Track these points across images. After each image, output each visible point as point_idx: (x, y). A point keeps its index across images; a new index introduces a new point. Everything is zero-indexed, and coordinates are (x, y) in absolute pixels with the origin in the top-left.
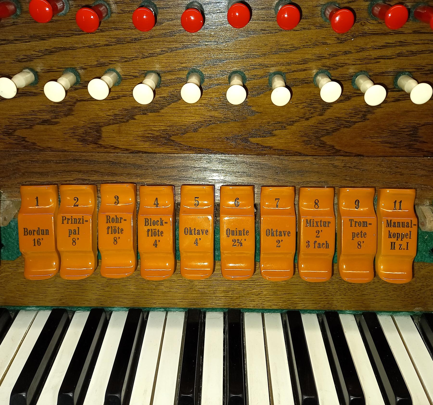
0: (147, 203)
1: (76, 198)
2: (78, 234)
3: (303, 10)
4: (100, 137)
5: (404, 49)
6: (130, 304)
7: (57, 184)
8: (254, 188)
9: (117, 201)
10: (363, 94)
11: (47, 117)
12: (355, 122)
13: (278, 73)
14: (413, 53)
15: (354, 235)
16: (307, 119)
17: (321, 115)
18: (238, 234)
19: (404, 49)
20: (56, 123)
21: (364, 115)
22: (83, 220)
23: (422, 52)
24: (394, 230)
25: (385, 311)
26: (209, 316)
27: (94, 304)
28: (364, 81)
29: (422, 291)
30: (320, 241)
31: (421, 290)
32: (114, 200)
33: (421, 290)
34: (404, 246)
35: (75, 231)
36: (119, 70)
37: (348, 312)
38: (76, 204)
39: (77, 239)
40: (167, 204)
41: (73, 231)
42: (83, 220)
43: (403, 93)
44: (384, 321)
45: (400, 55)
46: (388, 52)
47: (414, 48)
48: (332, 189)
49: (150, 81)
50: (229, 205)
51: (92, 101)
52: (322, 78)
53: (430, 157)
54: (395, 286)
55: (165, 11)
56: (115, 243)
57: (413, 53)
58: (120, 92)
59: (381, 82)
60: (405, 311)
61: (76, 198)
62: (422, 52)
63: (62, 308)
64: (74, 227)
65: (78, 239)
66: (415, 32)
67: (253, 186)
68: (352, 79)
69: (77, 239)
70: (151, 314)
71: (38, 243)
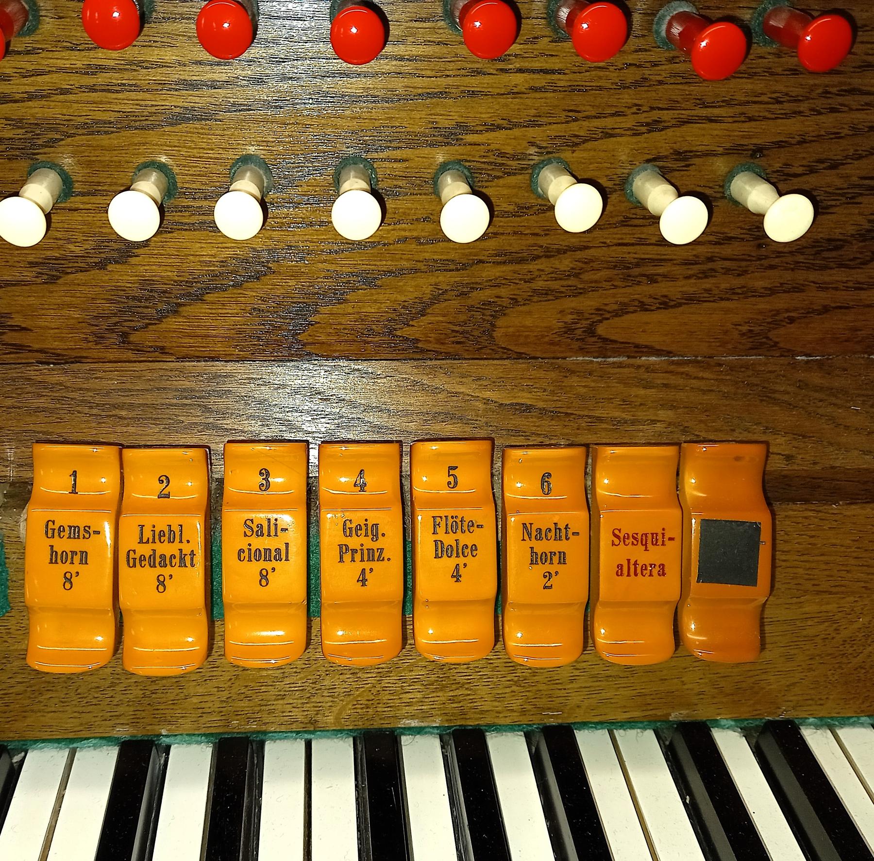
0: (143, 489)
1: (163, 478)
2: (287, 559)
3: (385, 8)
6: (214, 723)
7: (679, 444)
8: (401, 446)
9: (264, 482)
10: (655, 220)
13: (263, 166)
18: (366, 558)
22: (276, 529)
25: (44, 741)
26: (271, 749)
28: (154, 183)
29: (118, 688)
31: (113, 685)
32: (260, 479)
33: (113, 685)
35: (278, 550)
36: (67, 162)
37: (864, 719)
38: (166, 492)
39: (167, 578)
40: (190, 487)
41: (273, 553)
42: (276, 529)
44: (591, 745)
48: (486, 445)
49: (148, 187)
50: (339, 487)
51: (665, 245)
52: (454, 180)
53: (53, 363)
54: (47, 678)
55: (528, 21)
56: (264, 582)
59: (689, 190)
60: (95, 738)
61: (163, 478)
63: (235, 735)
65: (171, 576)
67: (400, 443)
68: (625, 182)
69: (167, 578)
70: (269, 747)
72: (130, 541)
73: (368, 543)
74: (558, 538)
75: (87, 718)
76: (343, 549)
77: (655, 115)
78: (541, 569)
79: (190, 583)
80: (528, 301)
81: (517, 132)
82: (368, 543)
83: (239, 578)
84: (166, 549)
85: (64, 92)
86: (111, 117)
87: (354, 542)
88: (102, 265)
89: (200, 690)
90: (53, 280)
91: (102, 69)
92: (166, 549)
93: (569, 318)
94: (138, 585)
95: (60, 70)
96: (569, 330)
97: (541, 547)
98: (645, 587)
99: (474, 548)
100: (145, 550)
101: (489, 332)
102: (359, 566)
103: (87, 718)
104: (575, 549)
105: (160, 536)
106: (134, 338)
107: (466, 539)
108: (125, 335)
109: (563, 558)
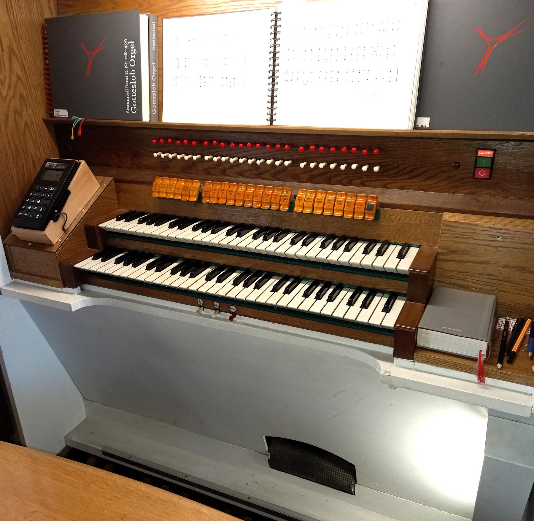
11: (214, 166)
104: (353, 205)
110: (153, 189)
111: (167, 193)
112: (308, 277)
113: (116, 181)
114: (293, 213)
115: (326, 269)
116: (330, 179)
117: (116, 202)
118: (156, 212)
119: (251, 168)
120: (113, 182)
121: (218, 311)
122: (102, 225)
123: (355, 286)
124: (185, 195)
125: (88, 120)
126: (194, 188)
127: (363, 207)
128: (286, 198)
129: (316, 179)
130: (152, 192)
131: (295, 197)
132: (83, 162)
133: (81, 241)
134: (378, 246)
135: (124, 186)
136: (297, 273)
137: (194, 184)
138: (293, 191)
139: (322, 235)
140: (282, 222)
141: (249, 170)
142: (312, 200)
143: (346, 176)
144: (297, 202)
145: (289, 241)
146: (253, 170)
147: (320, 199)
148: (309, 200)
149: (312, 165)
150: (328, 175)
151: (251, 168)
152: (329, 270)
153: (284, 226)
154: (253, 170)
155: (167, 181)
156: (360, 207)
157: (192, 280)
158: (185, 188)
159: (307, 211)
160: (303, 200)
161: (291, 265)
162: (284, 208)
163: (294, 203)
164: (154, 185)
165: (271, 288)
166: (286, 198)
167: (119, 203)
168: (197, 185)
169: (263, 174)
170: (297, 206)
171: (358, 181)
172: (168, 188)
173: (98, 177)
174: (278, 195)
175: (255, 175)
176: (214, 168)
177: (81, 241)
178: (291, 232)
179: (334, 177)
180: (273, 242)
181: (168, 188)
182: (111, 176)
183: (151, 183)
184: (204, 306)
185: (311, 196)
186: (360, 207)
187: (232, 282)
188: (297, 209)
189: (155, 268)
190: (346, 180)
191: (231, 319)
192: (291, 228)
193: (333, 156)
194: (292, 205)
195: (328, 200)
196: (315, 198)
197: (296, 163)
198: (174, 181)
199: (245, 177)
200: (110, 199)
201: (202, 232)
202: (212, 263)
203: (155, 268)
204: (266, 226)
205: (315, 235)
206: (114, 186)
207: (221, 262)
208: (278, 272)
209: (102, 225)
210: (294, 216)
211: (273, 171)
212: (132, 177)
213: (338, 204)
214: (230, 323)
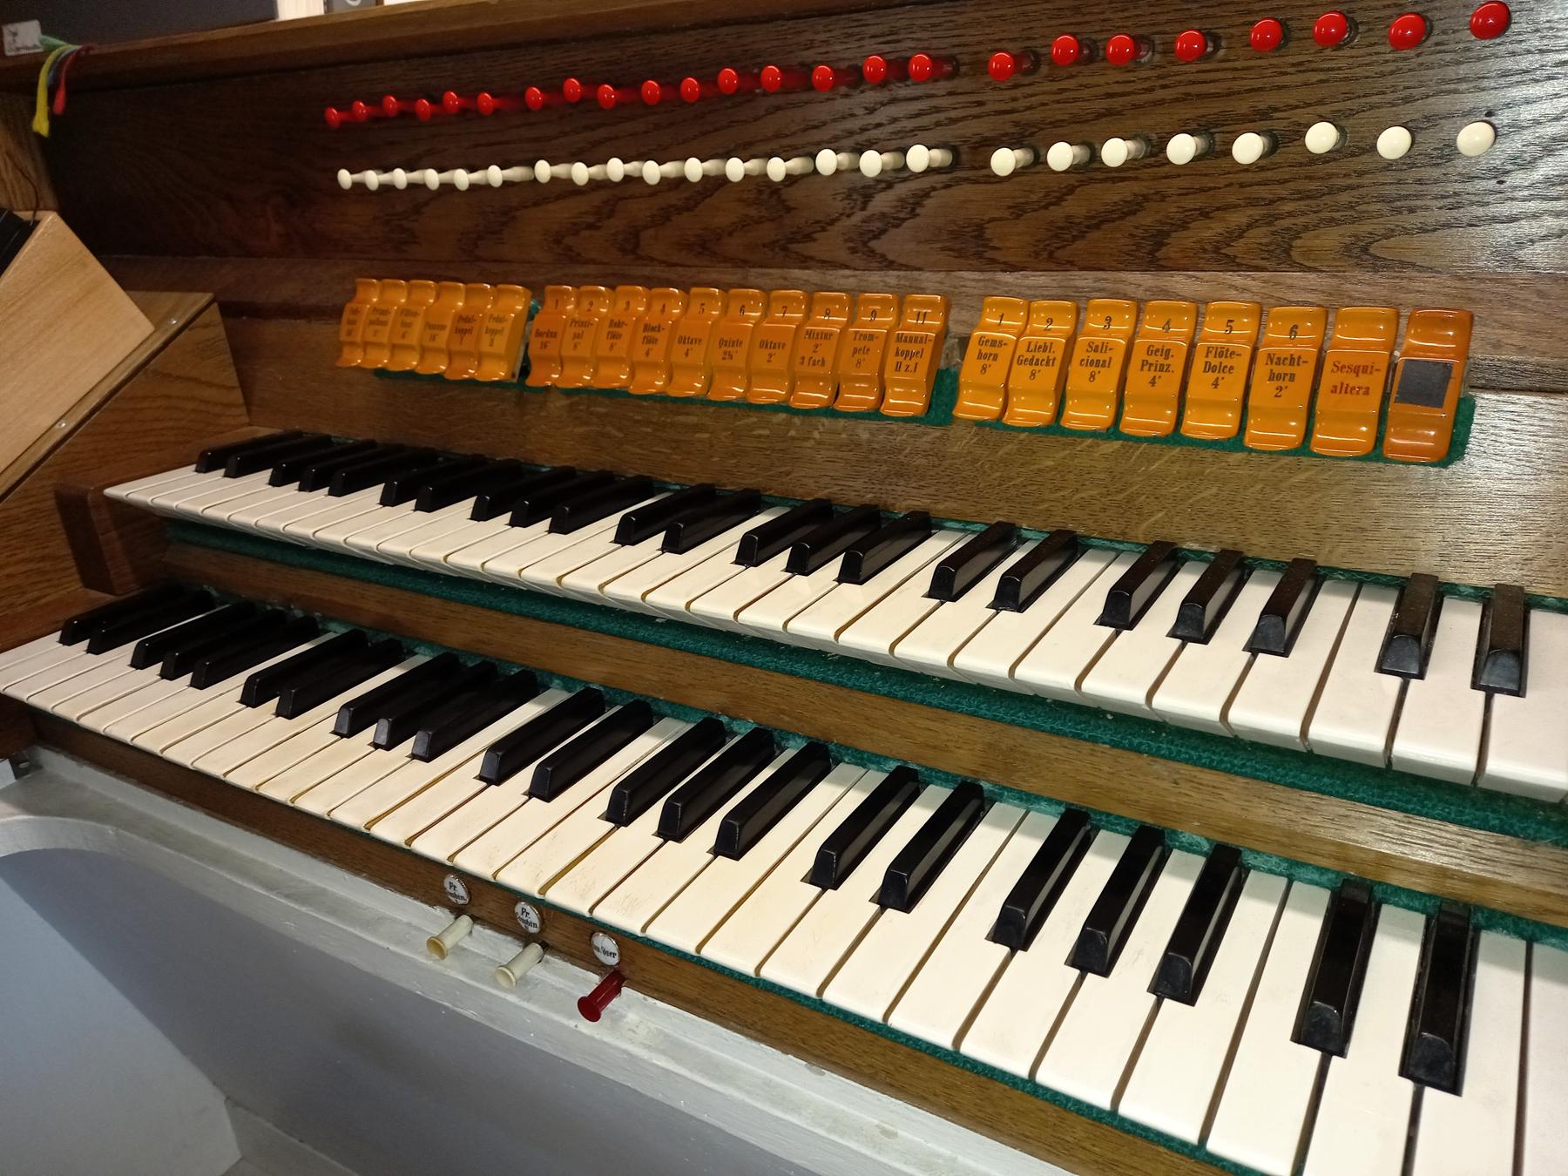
4: (637, 246)
5: (942, 116)
11: (591, 219)
12: (904, 220)
14: (953, 121)
15: (855, 351)
16: (849, 216)
17: (863, 209)
19: (942, 116)
20: (599, 228)
21: (913, 210)
23: (964, 118)
24: (903, 346)
27: (1072, 796)
30: (817, 357)
34: (912, 368)
43: (1166, 169)
45: (938, 124)
46: (924, 121)
47: (953, 114)
57: (953, 121)
58: (1216, 151)
62: (964, 118)
64: (579, 330)
66: (951, 94)
71: (544, 345)
72: (1021, 350)
73: (1161, 360)
74: (1292, 364)
75: (980, 507)
76: (1144, 363)
77: (1407, 92)
78: (1276, 383)
79: (1049, 376)
80: (1316, 226)
81: (1310, 110)
82: (1161, 360)
83: (1078, 378)
84: (1040, 356)
85: (1043, 104)
86: (1066, 117)
87: (1152, 359)
88: (1046, 207)
89: (1053, 496)
90: (1018, 217)
91: (1065, 90)
92: (1040, 356)
93: (1348, 240)
94: (1021, 373)
95: (1044, 93)
96: (1347, 248)
97: (1277, 369)
98: (1351, 403)
99: (1232, 368)
100: (1029, 356)
101: (1287, 251)
102: (1152, 374)
103: (980, 507)
104: (1305, 374)
105: (1038, 348)
106: (1058, 254)
107: (1226, 362)
108: (1051, 254)
109: (1292, 377)
110: (343, 337)
111: (424, 351)
112: (1025, 787)
113: (231, 310)
114: (955, 431)
115: (1137, 750)
116: (1159, 239)
117: (237, 396)
118: (370, 436)
119: (753, 212)
120: (214, 314)
121: (535, 949)
122: (111, 492)
123: (1322, 870)
124: (468, 354)
125: (98, 49)
126: (499, 320)
127: (1376, 382)
128: (914, 348)
129: (1079, 244)
130: (339, 348)
131: (964, 342)
132: (50, 221)
133: (43, 559)
134: (1184, 583)
135: (273, 331)
136: (964, 761)
137: (505, 301)
138: (954, 314)
139: (1111, 548)
140: (900, 475)
141: (744, 224)
142: (1058, 354)
143: (1256, 212)
144: (970, 370)
145: (925, 580)
146: (759, 221)
147: (1104, 347)
148: (1035, 356)
149: (1061, 155)
150: (1147, 218)
151: (753, 212)
152: (1156, 754)
153: (904, 500)
154: (759, 221)
155: (399, 295)
156: (1352, 380)
157: (856, 595)
158: (464, 324)
159: (1030, 411)
160: (1005, 354)
161: (926, 711)
162: (906, 400)
163: (955, 378)
164: (346, 316)
165: (806, 858)
166: (914, 348)
167: (248, 403)
168: (516, 302)
169: (809, 238)
170: (978, 387)
171: (1331, 238)
172: (407, 327)
173: (152, 295)
174: (871, 337)
175: (772, 245)
176: (591, 227)
177: (43, 559)
178: (942, 528)
179: (1184, 226)
180: (840, 580)
181: (407, 327)
182: (204, 290)
183: (335, 313)
184: (475, 912)
185: (1051, 325)
186: (1352, 380)
187: (602, 803)
188: (973, 404)
189: (838, 563)
190: (1259, 235)
191: (591, 1008)
192: (941, 507)
193: (1185, 98)
194: (943, 387)
195: (1151, 351)
196: (1071, 341)
197: (968, 158)
198: (427, 294)
199: (726, 260)
200: (196, 380)
201: (513, 524)
202: (552, 674)
203: (838, 563)
204: (821, 494)
205: (1065, 548)
206: (220, 331)
207: (594, 673)
208: (865, 744)
209: (111, 492)
210: (960, 443)
211: (858, 217)
212: (288, 291)
213: (1209, 368)
214: (585, 1026)
